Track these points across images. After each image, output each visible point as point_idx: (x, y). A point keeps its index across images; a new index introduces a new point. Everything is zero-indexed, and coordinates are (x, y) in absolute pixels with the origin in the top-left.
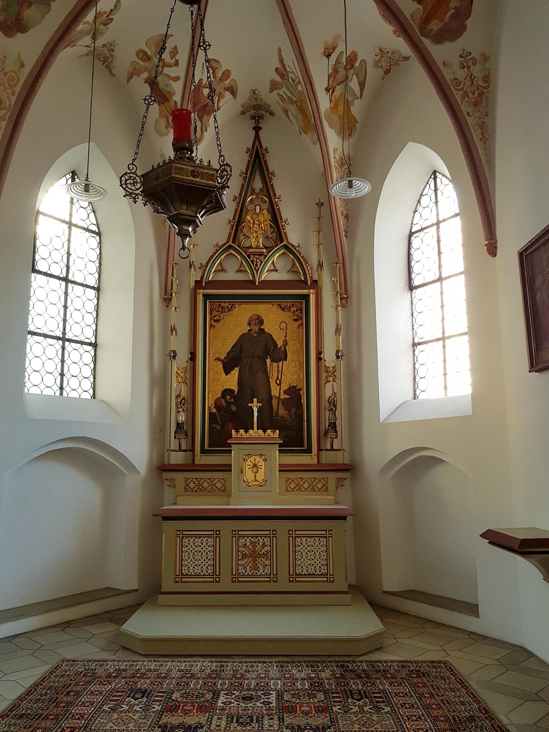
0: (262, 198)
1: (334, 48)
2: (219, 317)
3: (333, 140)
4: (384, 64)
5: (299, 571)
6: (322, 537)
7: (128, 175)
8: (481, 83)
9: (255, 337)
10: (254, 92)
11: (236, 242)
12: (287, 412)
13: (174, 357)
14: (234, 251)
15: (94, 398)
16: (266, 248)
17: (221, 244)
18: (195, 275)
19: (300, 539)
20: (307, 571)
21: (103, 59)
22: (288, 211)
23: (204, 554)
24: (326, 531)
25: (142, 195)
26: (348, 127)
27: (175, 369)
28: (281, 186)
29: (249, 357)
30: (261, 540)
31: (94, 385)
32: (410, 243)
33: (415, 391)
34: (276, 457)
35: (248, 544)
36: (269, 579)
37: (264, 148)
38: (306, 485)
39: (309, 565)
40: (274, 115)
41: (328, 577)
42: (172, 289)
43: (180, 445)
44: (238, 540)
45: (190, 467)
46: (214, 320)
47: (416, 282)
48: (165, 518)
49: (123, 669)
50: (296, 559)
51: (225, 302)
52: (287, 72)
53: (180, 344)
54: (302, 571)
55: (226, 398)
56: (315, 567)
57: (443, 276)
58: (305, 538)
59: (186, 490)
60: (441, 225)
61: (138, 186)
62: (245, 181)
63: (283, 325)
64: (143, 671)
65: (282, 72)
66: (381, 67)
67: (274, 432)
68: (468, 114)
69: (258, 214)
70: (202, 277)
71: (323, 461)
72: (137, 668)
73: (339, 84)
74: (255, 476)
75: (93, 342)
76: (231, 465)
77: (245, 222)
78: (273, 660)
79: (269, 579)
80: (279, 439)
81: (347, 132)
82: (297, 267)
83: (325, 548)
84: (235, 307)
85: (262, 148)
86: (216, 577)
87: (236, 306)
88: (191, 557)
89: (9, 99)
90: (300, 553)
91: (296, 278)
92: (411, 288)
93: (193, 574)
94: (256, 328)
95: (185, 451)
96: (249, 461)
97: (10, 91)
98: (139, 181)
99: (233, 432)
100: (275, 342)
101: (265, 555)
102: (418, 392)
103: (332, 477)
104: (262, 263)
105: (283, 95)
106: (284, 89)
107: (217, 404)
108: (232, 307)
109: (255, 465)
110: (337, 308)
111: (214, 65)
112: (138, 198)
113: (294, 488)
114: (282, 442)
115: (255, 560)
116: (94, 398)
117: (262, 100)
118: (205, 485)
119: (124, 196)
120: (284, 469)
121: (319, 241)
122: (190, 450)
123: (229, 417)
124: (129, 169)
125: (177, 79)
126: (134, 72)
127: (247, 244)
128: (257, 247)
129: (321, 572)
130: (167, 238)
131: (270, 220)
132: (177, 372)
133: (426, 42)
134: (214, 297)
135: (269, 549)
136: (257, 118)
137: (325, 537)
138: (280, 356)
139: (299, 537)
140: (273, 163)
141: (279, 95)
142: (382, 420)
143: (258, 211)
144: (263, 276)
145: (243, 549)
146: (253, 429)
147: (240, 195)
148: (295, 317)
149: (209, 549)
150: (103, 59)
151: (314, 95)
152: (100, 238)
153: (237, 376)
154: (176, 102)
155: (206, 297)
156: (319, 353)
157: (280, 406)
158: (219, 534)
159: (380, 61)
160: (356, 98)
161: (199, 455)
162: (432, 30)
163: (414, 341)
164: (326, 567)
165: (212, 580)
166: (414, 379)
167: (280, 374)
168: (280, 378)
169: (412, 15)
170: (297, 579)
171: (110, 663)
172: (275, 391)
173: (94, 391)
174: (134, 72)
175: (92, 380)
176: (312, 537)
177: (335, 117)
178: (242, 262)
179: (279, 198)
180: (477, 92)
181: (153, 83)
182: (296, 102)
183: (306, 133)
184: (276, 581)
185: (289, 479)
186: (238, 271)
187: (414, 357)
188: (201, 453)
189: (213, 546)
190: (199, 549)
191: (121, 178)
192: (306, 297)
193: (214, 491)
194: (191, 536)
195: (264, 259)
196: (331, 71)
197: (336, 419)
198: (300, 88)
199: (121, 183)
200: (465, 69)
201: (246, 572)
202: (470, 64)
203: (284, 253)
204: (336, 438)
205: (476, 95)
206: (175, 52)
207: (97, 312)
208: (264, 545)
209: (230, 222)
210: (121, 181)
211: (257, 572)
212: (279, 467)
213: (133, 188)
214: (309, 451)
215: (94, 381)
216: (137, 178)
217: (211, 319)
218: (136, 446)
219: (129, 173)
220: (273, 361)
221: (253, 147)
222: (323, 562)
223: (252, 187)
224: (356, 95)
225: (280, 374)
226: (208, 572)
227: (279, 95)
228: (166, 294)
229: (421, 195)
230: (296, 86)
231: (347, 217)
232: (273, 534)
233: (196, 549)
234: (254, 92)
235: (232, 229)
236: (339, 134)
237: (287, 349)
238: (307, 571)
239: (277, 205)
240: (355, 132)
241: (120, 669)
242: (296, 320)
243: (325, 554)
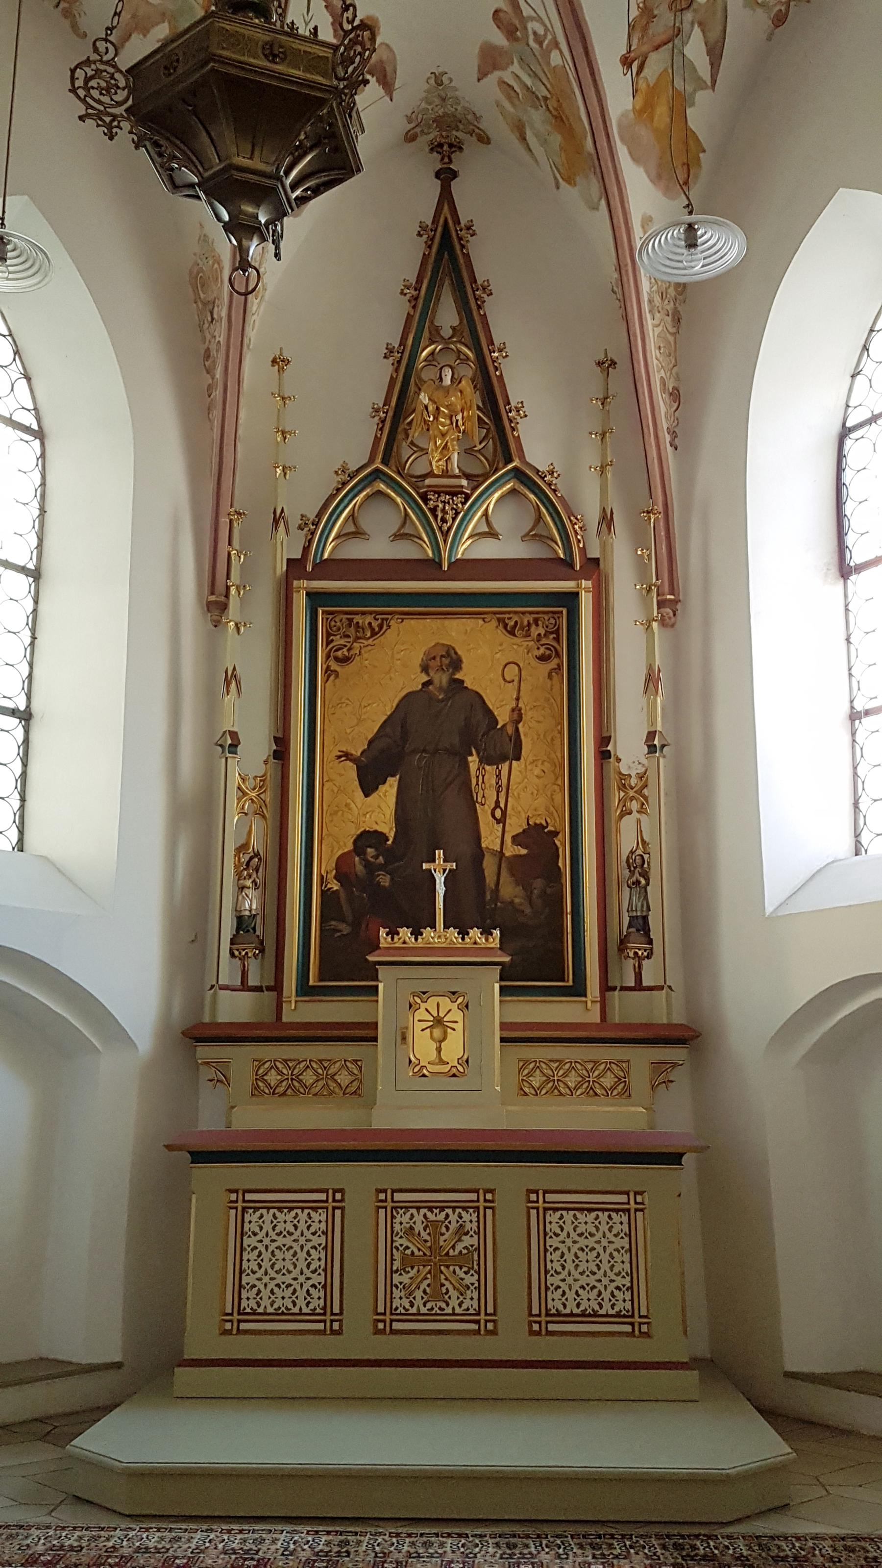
0: (459, 352)
2: (349, 650)
5: (555, 1302)
6: (617, 1211)
7: (93, 67)
9: (442, 701)
10: (438, 79)
11: (392, 462)
13: (233, 748)
14: (388, 486)
15: (21, 850)
16: (468, 477)
17: (353, 467)
18: (289, 546)
19: (558, 1214)
20: (578, 1305)
22: (526, 383)
23: (302, 1255)
24: (627, 1193)
25: (128, 119)
27: (235, 779)
28: (504, 322)
29: (424, 751)
30: (453, 1218)
31: (22, 817)
32: (840, 456)
33: (857, 835)
34: (497, 1008)
35: (419, 1227)
36: (475, 1327)
37: (463, 222)
38: (572, 1080)
39: (582, 1287)
40: (488, 142)
41: (636, 1324)
42: (228, 577)
44: (393, 1217)
45: (271, 1032)
46: (337, 659)
47: (857, 557)
48: (200, 1157)
49: (71, 1546)
50: (546, 1272)
51: (363, 613)
52: (524, 20)
53: (250, 716)
54: (565, 1306)
55: (365, 853)
56: (600, 1294)
58: (572, 1213)
59: (256, 1091)
61: (120, 96)
62: (414, 307)
63: (512, 672)
64: (126, 1551)
69: (447, 390)
70: (306, 549)
71: (616, 1017)
72: (110, 1544)
73: (657, 48)
74: (439, 1050)
75: (22, 707)
76: (376, 1024)
77: (414, 411)
78: (487, 1531)
79: (475, 1327)
80: (499, 952)
82: (546, 524)
84: (389, 627)
85: (459, 223)
86: (330, 1320)
87: (392, 623)
88: (266, 1265)
90: (558, 1253)
91: (545, 554)
92: (845, 571)
93: (270, 1310)
94: (441, 679)
95: (258, 989)
96: (422, 1010)
98: (122, 83)
99: (383, 932)
100: (489, 712)
101: (464, 1260)
102: (865, 839)
103: (641, 1059)
104: (457, 514)
105: (512, 82)
106: (516, 67)
108: (381, 627)
109: (438, 1021)
110: (649, 627)
112: (118, 127)
113: (541, 1088)
115: (436, 1273)
116: (21, 850)
117: (457, 101)
118: (309, 1078)
119: (81, 118)
120: (514, 1036)
121: (604, 456)
122: (269, 989)
123: (372, 899)
124: (96, 50)
127: (420, 469)
128: (446, 474)
129: (617, 1309)
130: (216, 450)
131: (479, 408)
132: (239, 788)
134: (334, 604)
135: (474, 1241)
136: (446, 147)
137: (623, 1210)
139: (555, 1210)
140: (487, 259)
141: (502, 83)
142: (769, 909)
143: (447, 381)
144: (461, 550)
145: (406, 1243)
146: (433, 926)
147: (403, 343)
148: (542, 650)
149: (316, 1240)
151: (593, 74)
152: (43, 444)
153: (393, 800)
155: (315, 598)
156: (603, 741)
158: (342, 1201)
160: (700, 85)
161: (293, 999)
163: (852, 708)
164: (628, 1296)
165: (321, 1326)
166: (856, 805)
167: (503, 795)
168: (502, 805)
170: (551, 1327)
171: (38, 1532)
172: (490, 837)
173: (21, 832)
175: (17, 804)
176: (590, 1210)
178: (406, 514)
179: (500, 351)
182: (546, 99)
183: (570, 181)
184: (494, 1333)
185: (526, 1062)
186: (399, 536)
187: (853, 747)
188: (297, 996)
189: (325, 1233)
190: (288, 1241)
191: (73, 71)
192: (571, 600)
193: (332, 1093)
194: (268, 1205)
195: (464, 504)
196: (634, 13)
197: (649, 909)
198: (555, 58)
199: (73, 84)
201: (412, 1305)
203: (513, 491)
204: (648, 957)
207: (33, 631)
208: (461, 1232)
209: (377, 411)
210: (73, 79)
211: (444, 1305)
212: (502, 1029)
213: (106, 99)
214: (578, 990)
215: (22, 807)
216: (117, 76)
217: (328, 657)
218: (128, 975)
219: (95, 62)
220: (486, 760)
221: (435, 220)
222: (619, 1281)
223: (432, 322)
224: (699, 78)
225: (503, 795)
226: (311, 1306)
228: (212, 593)
229: (872, 331)
230: (547, 54)
231: (675, 395)
232: (485, 1201)
233: (281, 1241)
234: (438, 79)
235: (381, 429)
236: (657, 178)
237: (521, 729)
238: (578, 1305)
239: (496, 369)
240: (696, 177)
241: (62, 1546)
242: (543, 658)
243: (627, 1258)
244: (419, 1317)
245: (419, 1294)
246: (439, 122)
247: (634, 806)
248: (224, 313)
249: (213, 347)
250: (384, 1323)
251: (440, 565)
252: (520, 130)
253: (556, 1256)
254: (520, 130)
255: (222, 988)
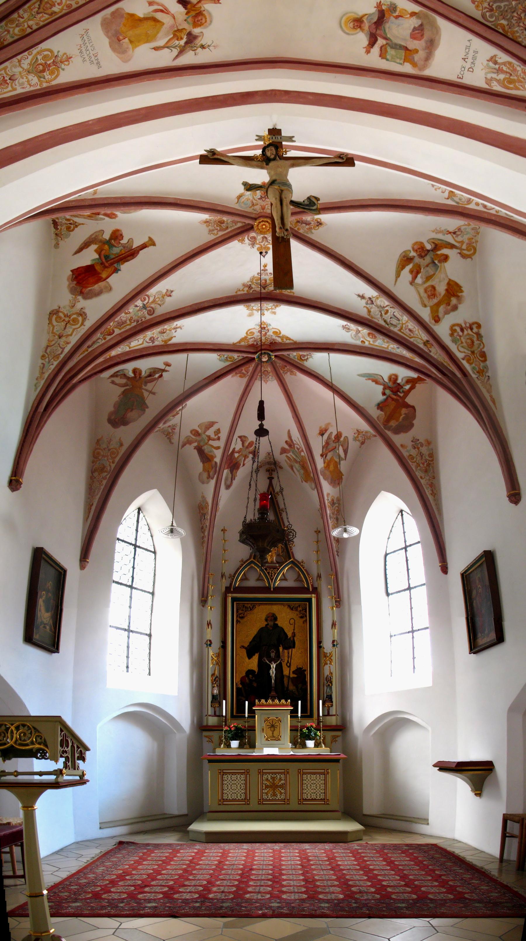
1: (326, 430)
3: (327, 487)
4: (360, 439)
5: (305, 797)
8: (427, 458)
12: (295, 688)
13: (210, 645)
16: (278, 563)
18: (225, 583)
21: (169, 435)
23: (239, 786)
26: (337, 478)
27: (211, 653)
32: (385, 561)
43: (215, 712)
47: (390, 591)
52: (294, 444)
53: (213, 634)
57: (411, 586)
60: (408, 549)
65: (290, 443)
66: (359, 440)
67: (286, 701)
68: (421, 477)
70: (231, 584)
73: (330, 452)
74: (273, 733)
81: (337, 482)
82: (301, 577)
83: (323, 782)
86: (246, 801)
88: (229, 788)
89: (110, 466)
94: (271, 623)
97: (111, 461)
99: (257, 701)
101: (282, 786)
106: (291, 453)
107: (242, 680)
108: (253, 607)
110: (333, 609)
111: (244, 439)
114: (292, 708)
115: (277, 786)
125: (218, 448)
126: (189, 442)
133: (389, 433)
135: (284, 782)
138: (290, 644)
141: (287, 456)
149: (242, 782)
150: (169, 435)
154: (216, 463)
155: (234, 600)
156: (319, 642)
157: (290, 683)
159: (357, 437)
160: (343, 460)
162: (391, 426)
169: (378, 418)
174: (189, 442)
177: (328, 473)
180: (425, 464)
181: (200, 451)
186: (258, 580)
192: (310, 600)
194: (229, 773)
196: (324, 444)
198: (302, 454)
200: (416, 449)
202: (419, 446)
203: (291, 567)
205: (425, 465)
206: (218, 432)
208: (280, 779)
220: (285, 648)
222: (322, 791)
227: (287, 456)
233: (233, 782)
242: (302, 617)
244: (269, 800)
245: (269, 795)
246: (269, 463)
247: (328, 662)
248: (209, 517)
249: (205, 526)
250: (261, 802)
251: (270, 589)
252: (292, 467)
253: (305, 785)
254: (292, 467)
255: (210, 716)
